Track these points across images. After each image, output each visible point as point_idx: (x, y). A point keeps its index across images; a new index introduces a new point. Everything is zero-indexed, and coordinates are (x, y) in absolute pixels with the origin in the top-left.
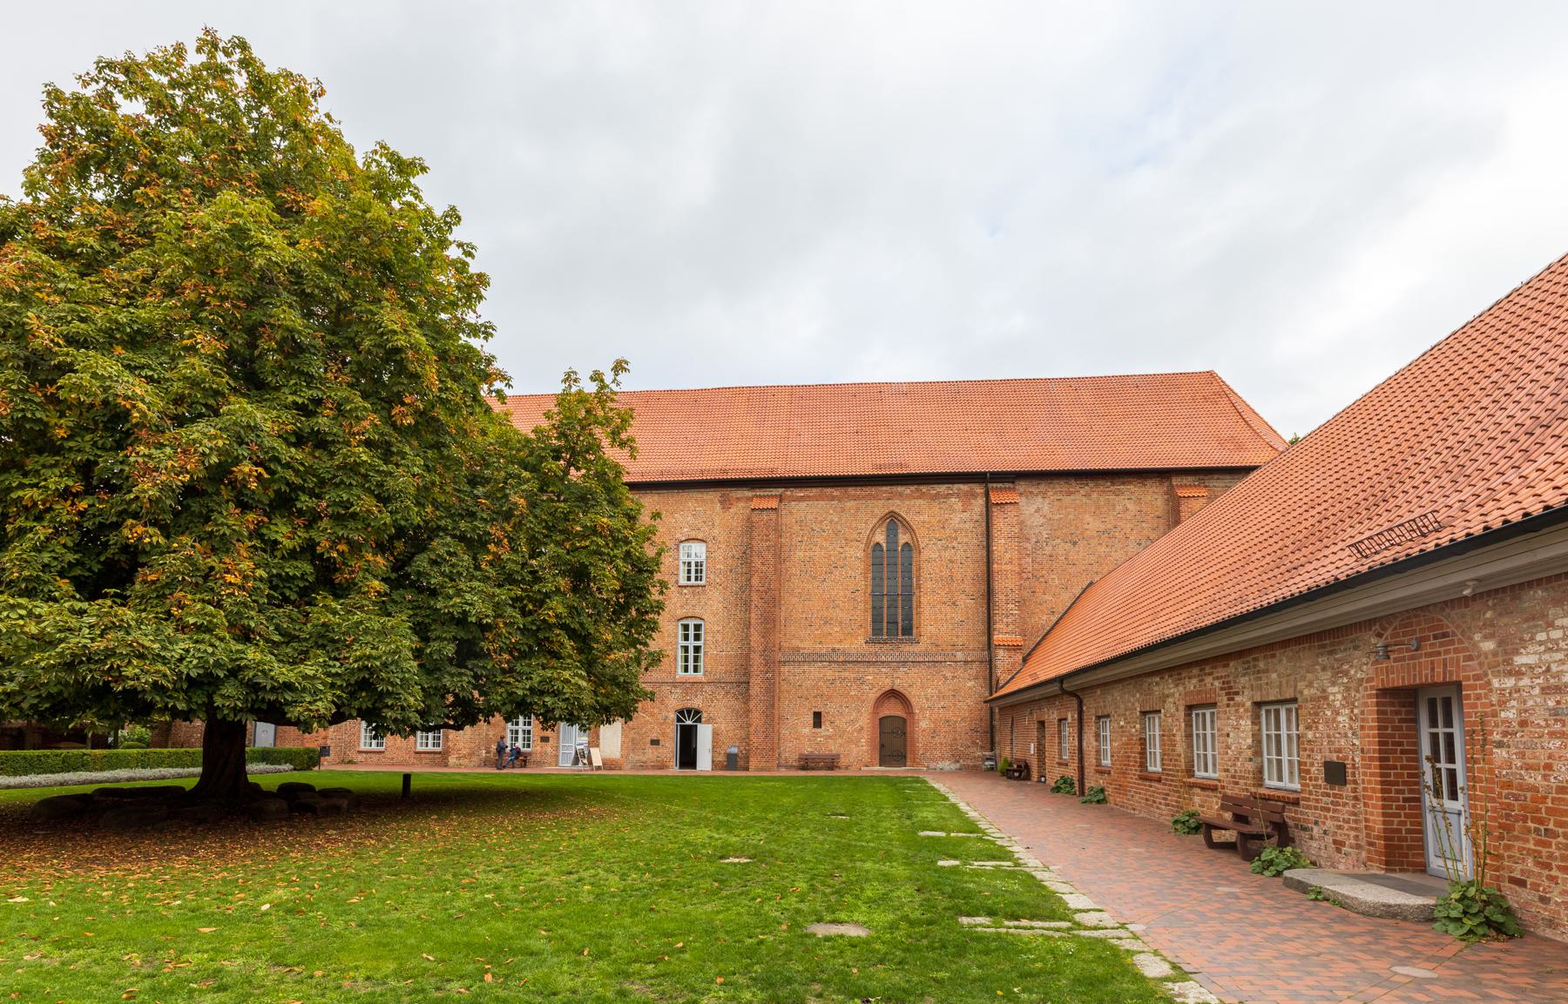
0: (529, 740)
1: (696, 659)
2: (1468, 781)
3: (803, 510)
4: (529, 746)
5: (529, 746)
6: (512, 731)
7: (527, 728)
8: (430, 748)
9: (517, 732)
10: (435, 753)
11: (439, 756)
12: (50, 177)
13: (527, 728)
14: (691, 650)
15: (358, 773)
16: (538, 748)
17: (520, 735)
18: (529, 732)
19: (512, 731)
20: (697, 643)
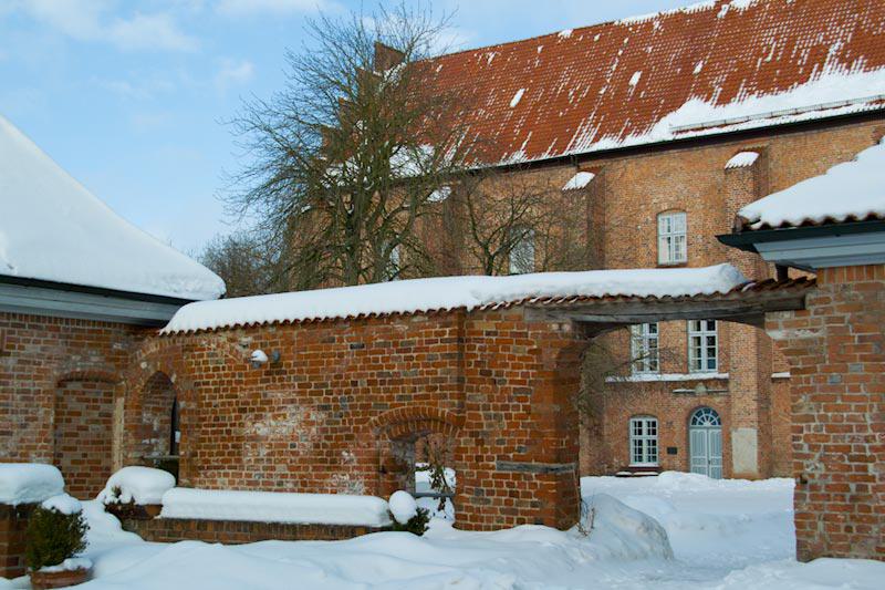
0: (654, 452)
1: (711, 352)
7: (652, 437)
9: (640, 442)
13: (652, 437)
17: (645, 446)
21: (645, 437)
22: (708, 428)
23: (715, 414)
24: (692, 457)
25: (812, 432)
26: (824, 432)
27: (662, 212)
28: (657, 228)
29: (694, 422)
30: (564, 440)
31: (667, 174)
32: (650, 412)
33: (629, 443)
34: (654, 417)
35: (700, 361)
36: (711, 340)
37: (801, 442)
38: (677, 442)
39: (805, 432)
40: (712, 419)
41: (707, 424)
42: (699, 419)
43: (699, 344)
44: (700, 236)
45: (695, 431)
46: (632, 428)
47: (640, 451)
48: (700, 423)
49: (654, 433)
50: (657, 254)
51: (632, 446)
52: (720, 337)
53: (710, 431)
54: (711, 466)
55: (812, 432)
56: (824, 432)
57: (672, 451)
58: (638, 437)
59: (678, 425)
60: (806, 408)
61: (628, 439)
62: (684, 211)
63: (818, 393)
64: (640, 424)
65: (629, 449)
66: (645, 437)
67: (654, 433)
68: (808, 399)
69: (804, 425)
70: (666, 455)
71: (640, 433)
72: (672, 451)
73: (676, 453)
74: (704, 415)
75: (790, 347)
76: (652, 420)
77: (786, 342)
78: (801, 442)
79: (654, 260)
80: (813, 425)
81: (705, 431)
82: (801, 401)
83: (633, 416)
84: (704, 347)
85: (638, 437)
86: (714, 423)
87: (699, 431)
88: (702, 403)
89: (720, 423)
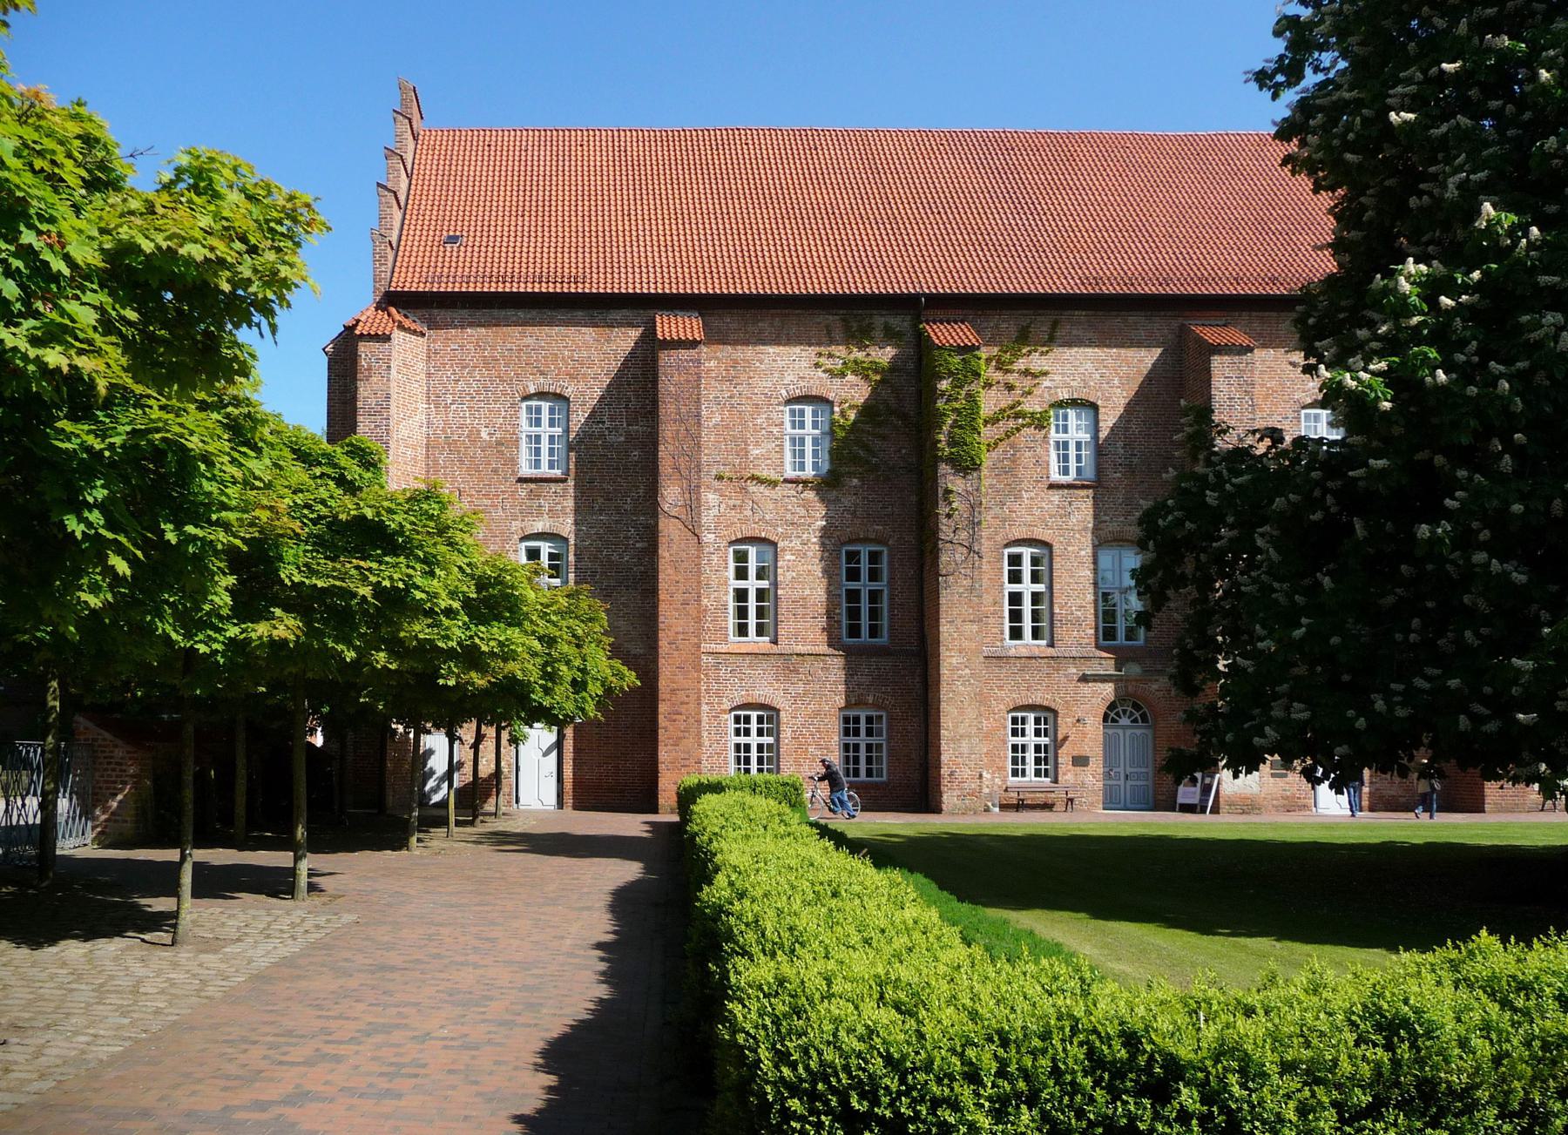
9: (538, 438)
18: (1015, 733)
20: (874, 740)
21: (1027, 588)
40: (1132, 714)
46: (523, 414)
47: (538, 452)
53: (1129, 732)
54: (1129, 783)
58: (874, 740)
64: (869, 773)
70: (1070, 767)
71: (869, 748)
81: (1120, 732)
84: (865, 622)
86: (1135, 721)
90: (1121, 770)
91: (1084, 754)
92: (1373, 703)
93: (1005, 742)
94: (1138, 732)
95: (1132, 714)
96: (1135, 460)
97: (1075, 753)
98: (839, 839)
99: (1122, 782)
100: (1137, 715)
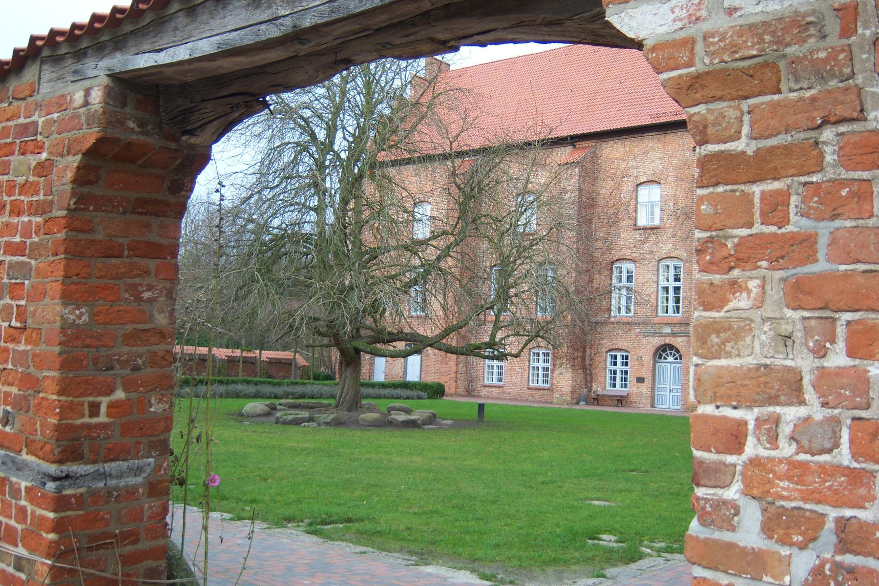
0: (626, 380)
1: (677, 301)
2: (39, 519)
3: (612, 150)
4: (626, 386)
5: (626, 386)
6: (489, 366)
7: (625, 368)
8: (541, 384)
9: (615, 372)
10: (543, 389)
11: (548, 392)
12: (767, 38)
13: (625, 368)
14: (671, 291)
15: (534, 407)
16: (634, 389)
17: (618, 376)
18: (626, 372)
19: (489, 366)
20: (677, 284)
21: (619, 367)
22: (671, 363)
23: (678, 351)
24: (657, 386)
25: (786, 449)
26: (844, 456)
27: (641, 184)
28: (637, 197)
29: (660, 358)
30: (104, 401)
31: (646, 153)
32: (624, 348)
33: (606, 373)
34: (627, 351)
35: (667, 307)
36: (677, 289)
37: (732, 493)
38: (646, 373)
39: (752, 448)
40: (674, 355)
41: (671, 359)
42: (664, 355)
43: (668, 293)
44: (671, 204)
45: (660, 365)
46: (609, 359)
47: (615, 379)
48: (665, 358)
49: (627, 364)
50: (636, 220)
51: (608, 375)
52: (684, 287)
53: (673, 365)
54: (672, 394)
55: (786, 449)
56: (844, 456)
57: (640, 380)
58: (613, 368)
59: (648, 359)
60: (764, 335)
61: (605, 368)
62: (659, 183)
63: (822, 265)
64: (616, 357)
65: (605, 377)
66: (619, 367)
67: (627, 364)
68: (775, 293)
69: (750, 416)
70: (635, 383)
71: (615, 364)
72: (640, 380)
73: (644, 382)
74: (668, 352)
75: (702, 63)
76: (625, 354)
77: (689, 43)
78: (732, 493)
79: (632, 222)
80: (791, 414)
81: (668, 365)
82: (741, 302)
83: (610, 350)
85: (613, 368)
86: (676, 359)
87: (663, 365)
88: (667, 342)
89: (681, 359)
90: (668, 386)
91: (642, 376)
92: (12, 408)
93: (631, 368)
94: (678, 365)
95: (674, 355)
96: (679, 212)
97: (638, 376)
98: (736, 60)
99: (668, 393)
100: (677, 355)
